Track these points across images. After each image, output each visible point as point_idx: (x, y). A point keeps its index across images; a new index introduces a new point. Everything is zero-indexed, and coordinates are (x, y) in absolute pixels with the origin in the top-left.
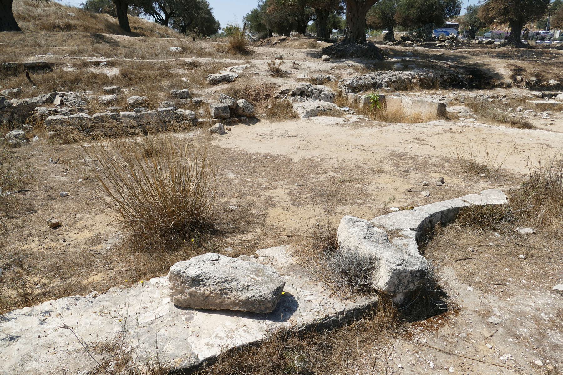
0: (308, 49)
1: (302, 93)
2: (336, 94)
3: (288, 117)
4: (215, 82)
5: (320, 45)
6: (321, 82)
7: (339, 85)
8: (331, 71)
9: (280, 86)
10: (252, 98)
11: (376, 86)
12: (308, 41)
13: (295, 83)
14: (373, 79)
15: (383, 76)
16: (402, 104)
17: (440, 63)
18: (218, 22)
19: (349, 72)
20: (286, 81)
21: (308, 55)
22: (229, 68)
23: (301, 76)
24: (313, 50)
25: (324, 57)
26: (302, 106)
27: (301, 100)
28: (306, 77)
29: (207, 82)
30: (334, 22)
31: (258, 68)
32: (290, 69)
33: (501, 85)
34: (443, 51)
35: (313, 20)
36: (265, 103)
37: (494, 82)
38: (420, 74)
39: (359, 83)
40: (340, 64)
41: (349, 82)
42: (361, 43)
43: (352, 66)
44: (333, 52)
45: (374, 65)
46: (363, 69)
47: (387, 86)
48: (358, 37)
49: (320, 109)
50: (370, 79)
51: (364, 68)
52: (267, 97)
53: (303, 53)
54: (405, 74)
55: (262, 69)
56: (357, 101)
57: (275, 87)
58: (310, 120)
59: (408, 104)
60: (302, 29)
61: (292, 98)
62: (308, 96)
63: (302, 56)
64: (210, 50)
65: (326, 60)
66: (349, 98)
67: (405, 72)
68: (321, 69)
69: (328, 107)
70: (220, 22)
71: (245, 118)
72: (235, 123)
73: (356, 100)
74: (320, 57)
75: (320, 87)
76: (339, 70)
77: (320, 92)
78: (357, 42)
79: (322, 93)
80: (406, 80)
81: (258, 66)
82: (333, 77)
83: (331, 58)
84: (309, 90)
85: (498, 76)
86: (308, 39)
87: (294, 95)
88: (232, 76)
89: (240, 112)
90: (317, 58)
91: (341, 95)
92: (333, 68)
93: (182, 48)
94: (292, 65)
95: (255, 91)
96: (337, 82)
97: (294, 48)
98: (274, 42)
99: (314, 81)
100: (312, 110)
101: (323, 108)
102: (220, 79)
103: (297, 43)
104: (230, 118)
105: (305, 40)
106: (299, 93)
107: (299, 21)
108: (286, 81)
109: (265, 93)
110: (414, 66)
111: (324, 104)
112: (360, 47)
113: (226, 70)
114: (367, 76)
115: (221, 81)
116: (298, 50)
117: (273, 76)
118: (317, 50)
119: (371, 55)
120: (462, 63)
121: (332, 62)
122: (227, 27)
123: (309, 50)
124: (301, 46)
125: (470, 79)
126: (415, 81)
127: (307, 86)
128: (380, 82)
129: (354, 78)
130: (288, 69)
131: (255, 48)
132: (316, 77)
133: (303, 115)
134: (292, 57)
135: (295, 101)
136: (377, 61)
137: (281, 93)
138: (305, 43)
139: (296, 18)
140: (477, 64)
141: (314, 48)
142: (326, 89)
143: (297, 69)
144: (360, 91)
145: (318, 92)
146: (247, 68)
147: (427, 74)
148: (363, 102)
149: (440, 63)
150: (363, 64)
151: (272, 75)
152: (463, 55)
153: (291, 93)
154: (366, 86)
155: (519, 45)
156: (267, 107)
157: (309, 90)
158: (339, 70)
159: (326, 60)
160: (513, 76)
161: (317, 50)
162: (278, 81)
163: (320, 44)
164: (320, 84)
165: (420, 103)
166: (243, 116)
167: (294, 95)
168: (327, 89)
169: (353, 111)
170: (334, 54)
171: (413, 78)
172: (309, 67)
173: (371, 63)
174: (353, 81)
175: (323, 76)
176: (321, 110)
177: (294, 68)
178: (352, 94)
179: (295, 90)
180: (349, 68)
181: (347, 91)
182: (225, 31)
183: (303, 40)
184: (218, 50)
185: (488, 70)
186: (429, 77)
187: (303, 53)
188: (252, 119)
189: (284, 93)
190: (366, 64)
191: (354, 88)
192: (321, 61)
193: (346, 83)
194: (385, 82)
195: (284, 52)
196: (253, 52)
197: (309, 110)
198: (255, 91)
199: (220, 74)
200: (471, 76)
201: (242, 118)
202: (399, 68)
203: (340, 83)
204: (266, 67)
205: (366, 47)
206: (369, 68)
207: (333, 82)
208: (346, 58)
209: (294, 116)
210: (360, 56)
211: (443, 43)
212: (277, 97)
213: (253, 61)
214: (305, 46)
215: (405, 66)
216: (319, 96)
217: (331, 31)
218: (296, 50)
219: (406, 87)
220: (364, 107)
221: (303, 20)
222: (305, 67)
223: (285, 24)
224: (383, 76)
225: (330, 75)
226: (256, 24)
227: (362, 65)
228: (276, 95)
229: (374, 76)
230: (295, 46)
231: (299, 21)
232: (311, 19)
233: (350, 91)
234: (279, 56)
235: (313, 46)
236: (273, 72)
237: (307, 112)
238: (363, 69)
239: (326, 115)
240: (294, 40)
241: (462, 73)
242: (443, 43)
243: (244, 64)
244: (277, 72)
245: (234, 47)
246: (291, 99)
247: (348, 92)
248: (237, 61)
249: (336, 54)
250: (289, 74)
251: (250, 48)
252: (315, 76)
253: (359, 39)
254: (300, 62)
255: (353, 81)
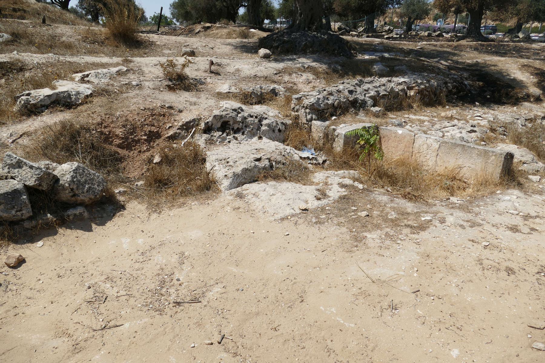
0: (237, 39)
1: (226, 126)
2: (289, 122)
3: (192, 186)
4: (32, 110)
5: (254, 35)
6: (261, 99)
7: (293, 106)
8: (276, 78)
9: (180, 111)
10: (117, 141)
11: (355, 106)
12: (237, 29)
13: (212, 102)
14: (351, 92)
15: (366, 86)
16: (416, 145)
17: (433, 62)
18: (142, 9)
19: (308, 81)
20: (194, 100)
21: (236, 47)
22: (80, 75)
23: (224, 88)
24: (244, 40)
25: (263, 51)
26: (225, 157)
27: (224, 139)
28: (233, 90)
29: (15, 109)
30: (266, 12)
31: (142, 73)
32: (205, 74)
33: (527, 98)
34: (420, 45)
35: (245, 6)
36: (148, 150)
37: (516, 93)
38: (419, 81)
39: (330, 102)
40: (289, 63)
41: (312, 100)
42: (316, 30)
43: (308, 68)
44: (276, 44)
45: (342, 66)
46: (327, 73)
47: (374, 105)
48: (311, 22)
49: (261, 165)
50: (346, 93)
51: (327, 70)
52: (153, 136)
53: (229, 44)
54: (398, 83)
55: (149, 76)
56: (329, 137)
57: (171, 115)
58: (240, 196)
59: (429, 147)
60: (232, 16)
61: (205, 136)
62: (237, 131)
63: (227, 49)
64: (72, 40)
65: (266, 57)
66: (313, 130)
67: (395, 79)
68: (259, 74)
69: (279, 158)
70: (144, 9)
71: (79, 210)
72: (48, 231)
73: (326, 135)
74: (256, 52)
75: (258, 109)
76: (290, 74)
77: (260, 121)
78: (310, 29)
79: (265, 122)
80: (401, 93)
81: (145, 69)
82: (280, 88)
83: (273, 53)
84: (239, 119)
85: (515, 84)
86: (239, 26)
87: (208, 129)
88: (78, 93)
89: (65, 196)
90: (251, 52)
91: (298, 124)
92: (279, 72)
93: (13, 34)
94: (208, 67)
95: (124, 126)
96: (288, 100)
97: (220, 37)
98: (197, 31)
99: (248, 98)
100: (245, 170)
101: (267, 163)
102: (48, 102)
103: (225, 31)
104: (30, 218)
105: (234, 28)
106: (219, 125)
107: (228, 7)
108: (194, 100)
109: (147, 129)
110: (404, 67)
111: (269, 147)
112: (317, 37)
113: (72, 79)
114: (341, 87)
115: (47, 107)
116: (222, 41)
117: (171, 88)
118: (250, 40)
119: (334, 50)
120: (457, 62)
121: (276, 60)
122: (154, 16)
123: (239, 40)
124: (229, 35)
125: (480, 87)
126: (412, 93)
127: (235, 110)
128: (362, 98)
129: (320, 92)
130: (200, 75)
131: (154, 37)
132: (250, 90)
133: (226, 183)
134: (211, 52)
135: (210, 142)
136: (344, 59)
137: (181, 128)
138: (234, 31)
139: (225, 4)
140: (477, 64)
141: (246, 38)
142: (271, 114)
143: (218, 74)
144: (332, 115)
145: (256, 121)
146: (119, 73)
147: (428, 81)
148: (342, 141)
149: (433, 62)
150: (325, 64)
151: (168, 86)
152: (445, 49)
153: (202, 126)
154: (341, 107)
155: (479, 37)
156: (150, 161)
157: (239, 119)
158: (290, 74)
159: (266, 57)
160: (538, 83)
161: (250, 40)
162: (180, 99)
163: (254, 33)
164: (259, 103)
165: (458, 149)
166: (75, 205)
167: (208, 129)
168: (271, 113)
169: (324, 158)
170: (277, 47)
171: (410, 88)
172: (238, 70)
173: (337, 63)
174: (319, 99)
175: (264, 86)
176: (264, 168)
177: (212, 72)
178: (318, 123)
179: (210, 119)
180: (304, 71)
181: (309, 117)
182: (152, 20)
183: (232, 27)
184: (85, 39)
185: (500, 73)
186: (431, 86)
187: (229, 44)
188: (102, 208)
189: (187, 127)
190: (329, 64)
191: (321, 112)
192: (258, 59)
193: (306, 102)
194: (371, 97)
195: (199, 44)
196: (152, 44)
197: (238, 170)
198: (124, 126)
199: (54, 88)
200: (481, 83)
201: (71, 212)
202: (382, 70)
203: (294, 101)
204: (159, 72)
205: (326, 37)
206: (335, 71)
207: (281, 99)
208: (296, 54)
209: (208, 186)
210: (317, 51)
211: (391, 35)
212: (173, 138)
213: (137, 59)
214: (234, 36)
215: (391, 70)
216: (259, 129)
217: (263, 21)
218: (219, 40)
219: (401, 104)
220: (345, 151)
221: (233, 6)
222: (231, 69)
223: (214, 11)
224: (366, 86)
225: (276, 86)
226: (183, 12)
227: (324, 67)
228: (171, 133)
229: (352, 88)
230: (222, 35)
231: (228, 7)
232: (242, 6)
233: (314, 117)
234: (188, 50)
235: (245, 35)
236: (170, 80)
237: (235, 175)
238: (327, 73)
239: (276, 178)
240: (221, 27)
241: (466, 79)
242: (391, 35)
243: (117, 64)
244: (178, 82)
245: (115, 35)
246: (201, 140)
247: (311, 120)
248: (105, 60)
249: (280, 47)
250: (202, 83)
251: (143, 36)
252: (249, 87)
253: (313, 24)
254: (224, 61)
255: (319, 99)
